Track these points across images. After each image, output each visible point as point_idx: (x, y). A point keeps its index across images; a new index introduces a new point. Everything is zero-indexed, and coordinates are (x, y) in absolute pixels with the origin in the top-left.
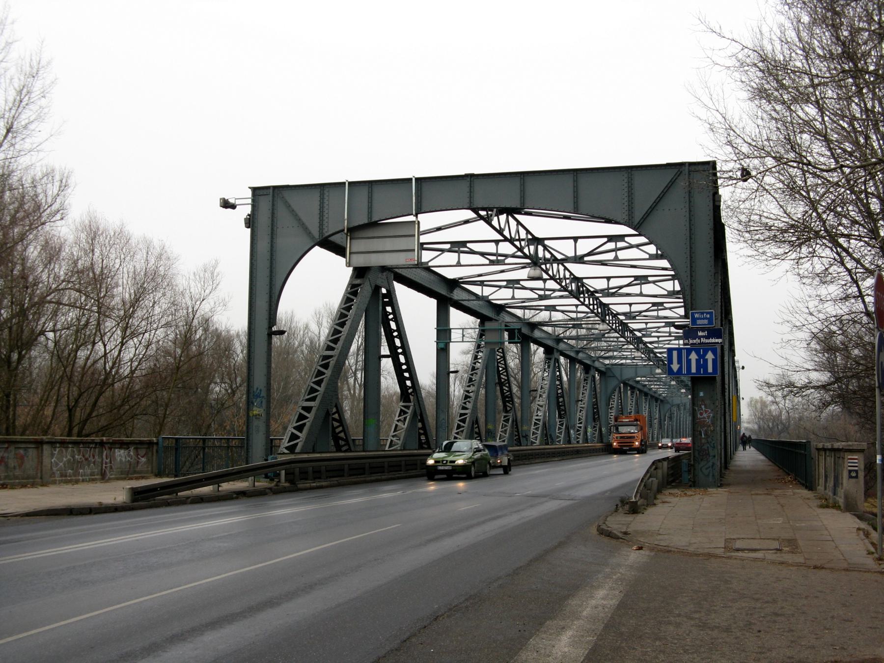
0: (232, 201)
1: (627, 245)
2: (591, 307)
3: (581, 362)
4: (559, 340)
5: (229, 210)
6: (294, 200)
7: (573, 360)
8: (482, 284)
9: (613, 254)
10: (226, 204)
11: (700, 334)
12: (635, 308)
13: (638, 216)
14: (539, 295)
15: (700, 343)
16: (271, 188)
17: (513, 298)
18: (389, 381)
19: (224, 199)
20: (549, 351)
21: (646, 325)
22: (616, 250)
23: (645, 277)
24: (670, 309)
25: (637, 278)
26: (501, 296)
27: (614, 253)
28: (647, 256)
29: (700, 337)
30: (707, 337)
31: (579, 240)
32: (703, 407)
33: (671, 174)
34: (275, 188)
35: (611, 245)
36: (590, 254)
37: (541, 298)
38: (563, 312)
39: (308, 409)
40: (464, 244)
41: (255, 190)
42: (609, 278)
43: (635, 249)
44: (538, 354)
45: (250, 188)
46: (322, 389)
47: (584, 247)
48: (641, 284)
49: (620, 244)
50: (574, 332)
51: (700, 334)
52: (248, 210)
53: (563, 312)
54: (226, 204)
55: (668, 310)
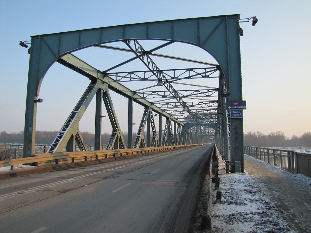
2: (182, 103)
3: (177, 122)
4: (177, 119)
5: (24, 47)
7: (175, 122)
8: (159, 103)
10: (22, 44)
11: (235, 104)
13: (203, 37)
14: (156, 93)
15: (235, 109)
16: (40, 36)
17: (167, 107)
19: (21, 42)
20: (168, 119)
24: (205, 104)
25: (200, 102)
26: (164, 107)
28: (205, 96)
29: (235, 105)
30: (238, 106)
32: (292, 217)
34: (41, 36)
35: (196, 93)
36: (190, 95)
37: (175, 107)
38: (179, 112)
40: (168, 103)
41: (33, 37)
42: (197, 110)
43: (204, 104)
44: (164, 119)
45: (31, 36)
47: (188, 93)
49: (198, 92)
50: (181, 117)
51: (235, 104)
53: (179, 112)
54: (22, 44)
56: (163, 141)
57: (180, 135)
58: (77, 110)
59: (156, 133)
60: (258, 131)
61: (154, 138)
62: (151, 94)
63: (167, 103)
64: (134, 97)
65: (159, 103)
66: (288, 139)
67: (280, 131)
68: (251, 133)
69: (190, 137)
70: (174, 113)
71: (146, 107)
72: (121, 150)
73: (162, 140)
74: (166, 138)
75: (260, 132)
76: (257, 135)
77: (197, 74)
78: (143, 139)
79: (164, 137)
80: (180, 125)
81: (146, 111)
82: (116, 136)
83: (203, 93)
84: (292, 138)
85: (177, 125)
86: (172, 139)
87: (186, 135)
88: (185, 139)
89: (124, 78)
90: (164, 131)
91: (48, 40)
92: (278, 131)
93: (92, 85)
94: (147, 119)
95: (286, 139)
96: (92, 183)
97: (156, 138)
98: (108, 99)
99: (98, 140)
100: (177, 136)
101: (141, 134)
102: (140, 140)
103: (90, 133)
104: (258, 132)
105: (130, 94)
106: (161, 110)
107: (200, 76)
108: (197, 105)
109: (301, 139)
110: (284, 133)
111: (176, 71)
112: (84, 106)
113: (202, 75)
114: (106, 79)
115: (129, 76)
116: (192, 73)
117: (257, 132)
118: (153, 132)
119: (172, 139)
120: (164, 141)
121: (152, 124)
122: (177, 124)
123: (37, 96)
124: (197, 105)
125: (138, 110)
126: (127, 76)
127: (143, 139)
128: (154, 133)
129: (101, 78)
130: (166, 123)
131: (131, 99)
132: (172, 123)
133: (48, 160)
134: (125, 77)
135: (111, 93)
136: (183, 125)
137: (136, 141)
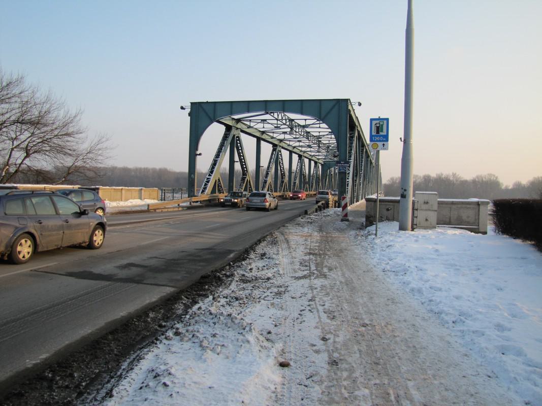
0: (184, 107)
3: (313, 160)
6: (203, 105)
7: (310, 160)
10: (182, 108)
12: (321, 134)
17: (264, 127)
18: (237, 166)
20: (300, 156)
30: (344, 164)
31: (307, 121)
33: (334, 102)
34: (199, 102)
39: (348, 179)
40: (265, 120)
41: (192, 103)
52: (189, 110)
54: (182, 108)
56: (293, 186)
57: (318, 178)
58: (218, 158)
59: (285, 176)
60: (454, 173)
61: (282, 182)
63: (264, 121)
64: (262, 137)
65: (250, 120)
66: (506, 187)
67: (491, 174)
68: (442, 175)
69: (333, 180)
70: (297, 144)
71: (275, 146)
72: (220, 195)
73: (292, 184)
74: (297, 182)
75: (457, 174)
76: (451, 179)
78: (219, 180)
79: (295, 180)
80: (318, 164)
81: (274, 150)
82: (246, 179)
84: (513, 186)
85: (314, 164)
86: (305, 183)
87: (326, 177)
88: (325, 184)
90: (294, 174)
91: (203, 105)
92: (488, 174)
93: (228, 133)
94: (276, 159)
95: (503, 187)
97: (285, 181)
98: (240, 143)
99: (231, 184)
100: (313, 179)
101: (268, 177)
102: (268, 184)
103: (171, 170)
104: (454, 175)
105: (258, 134)
106: (260, 131)
109: (529, 187)
110: (499, 178)
112: (224, 153)
114: (239, 125)
117: (453, 173)
118: (282, 174)
119: (305, 183)
120: (295, 186)
121: (280, 165)
122: (313, 163)
123: (197, 150)
125: (266, 149)
127: (219, 180)
128: (283, 175)
129: (235, 125)
130: (298, 162)
131: (259, 140)
132: (306, 161)
135: (243, 136)
136: (323, 163)
137: (264, 185)
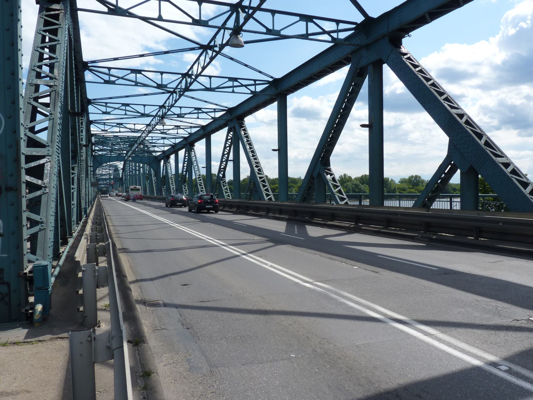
1: (173, 114)
9: (340, 28)
14: (123, 125)
17: (177, 133)
21: (338, 25)
22: (233, 87)
23: (179, 126)
24: (206, 113)
27: (232, 88)
35: (230, 84)
36: (218, 88)
46: (245, 140)
48: (177, 129)
49: (236, 84)
55: (182, 129)
62: (115, 126)
77: (321, 31)
83: (246, 86)
89: (117, 110)
95: (397, 181)
96: (204, 302)
107: (244, 82)
108: (190, 113)
111: (212, 78)
113: (201, 111)
115: (123, 108)
116: (312, 28)
124: (190, 113)
126: (120, 108)
133: (122, 321)
134: (118, 109)
